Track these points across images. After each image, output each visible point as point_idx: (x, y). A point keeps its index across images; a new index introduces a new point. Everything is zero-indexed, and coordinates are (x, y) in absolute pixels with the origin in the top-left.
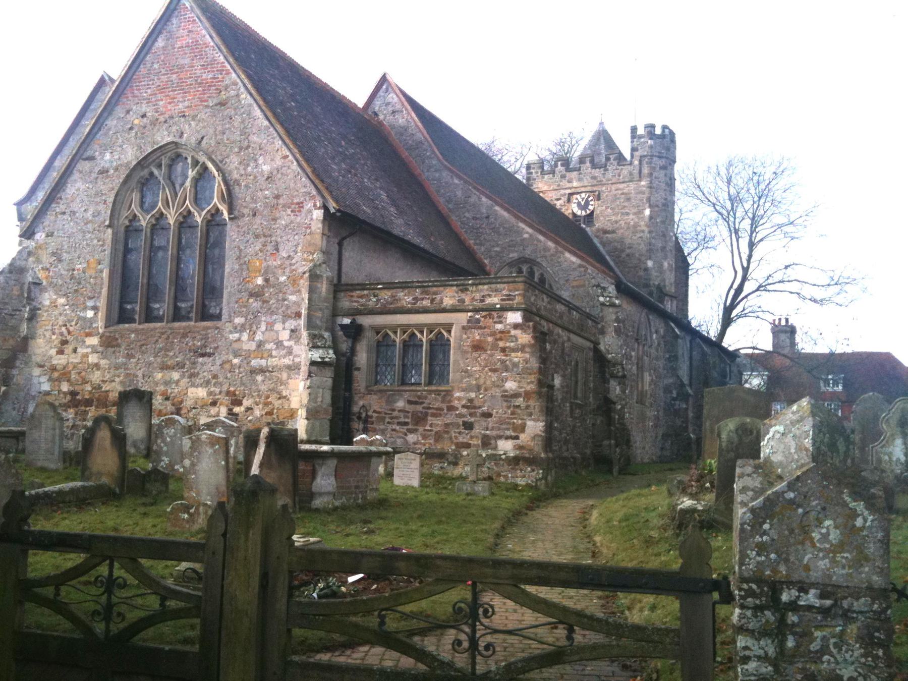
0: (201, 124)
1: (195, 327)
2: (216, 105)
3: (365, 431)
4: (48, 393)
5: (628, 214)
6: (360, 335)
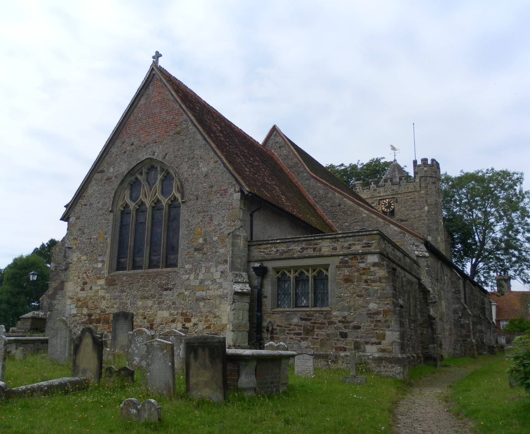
0: (165, 146)
1: (161, 271)
2: (175, 134)
3: (272, 339)
4: (75, 316)
5: (415, 210)
6: (266, 274)
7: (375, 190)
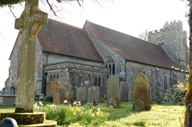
5: (170, 42)
7: (156, 35)
